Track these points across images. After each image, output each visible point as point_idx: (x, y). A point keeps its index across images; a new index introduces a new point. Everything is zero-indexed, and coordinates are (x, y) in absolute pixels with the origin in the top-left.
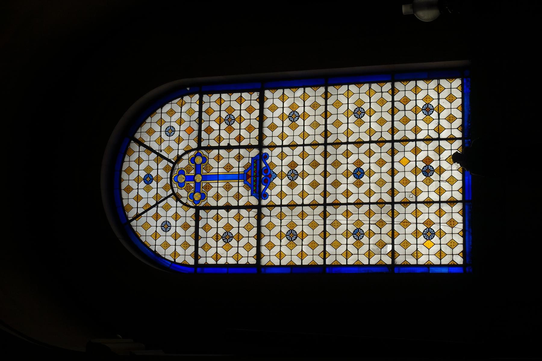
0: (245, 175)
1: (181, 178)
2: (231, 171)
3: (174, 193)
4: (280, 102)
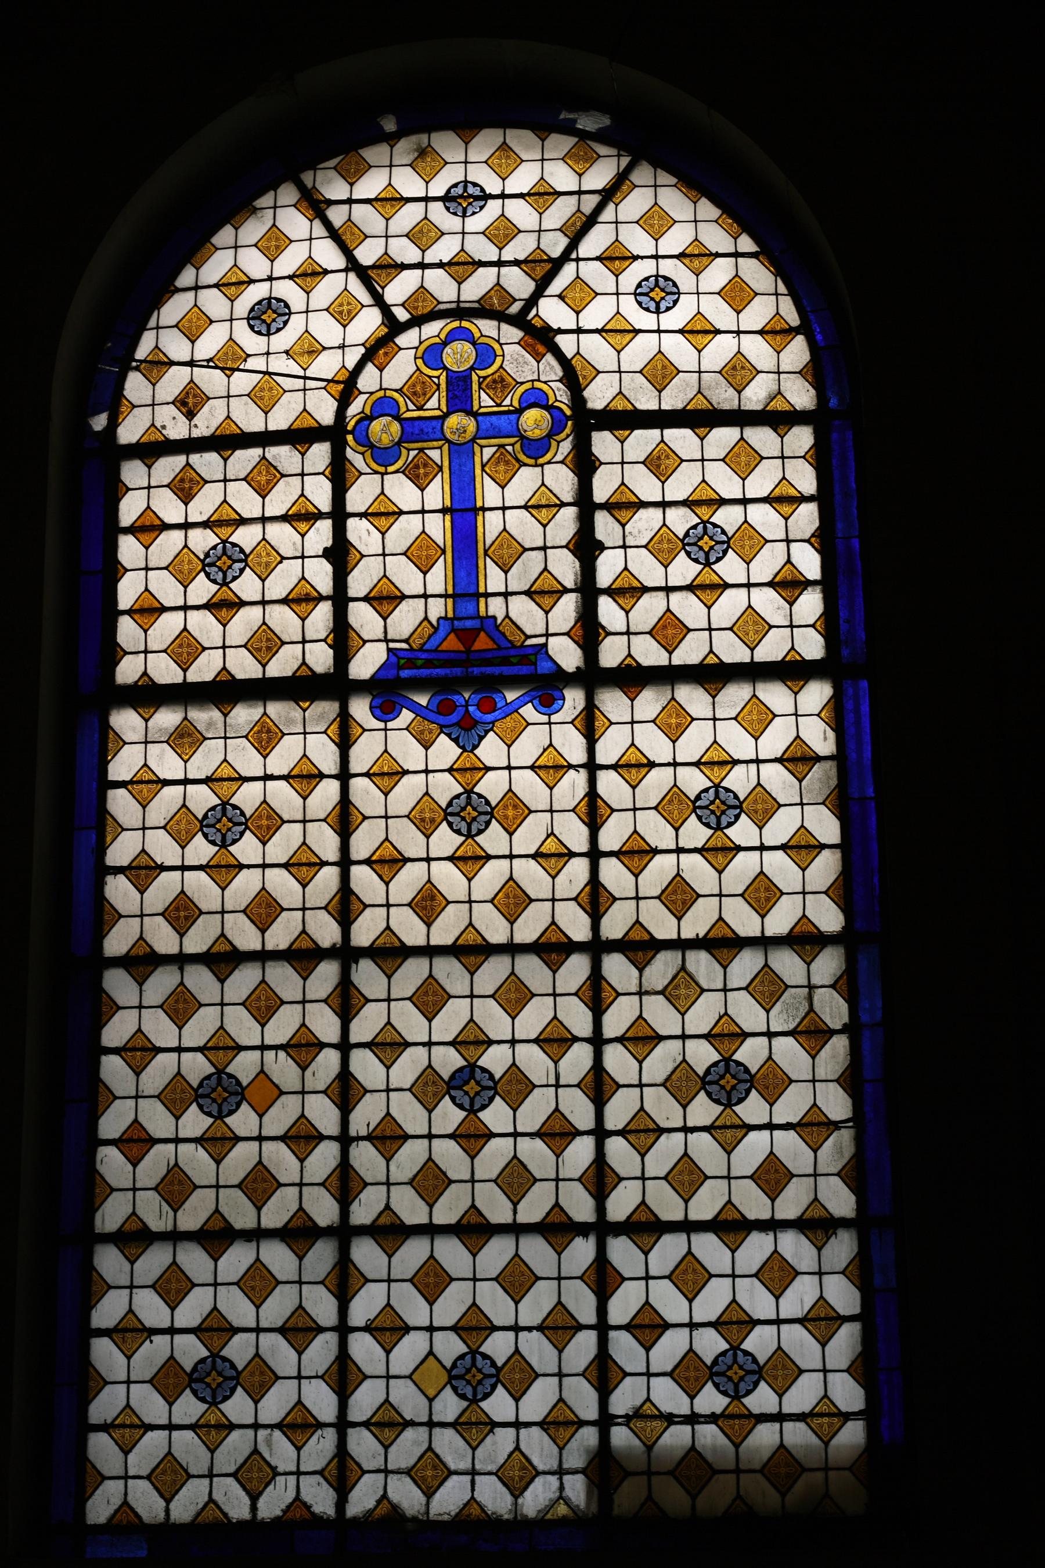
1: (459, 356)
3: (394, 327)
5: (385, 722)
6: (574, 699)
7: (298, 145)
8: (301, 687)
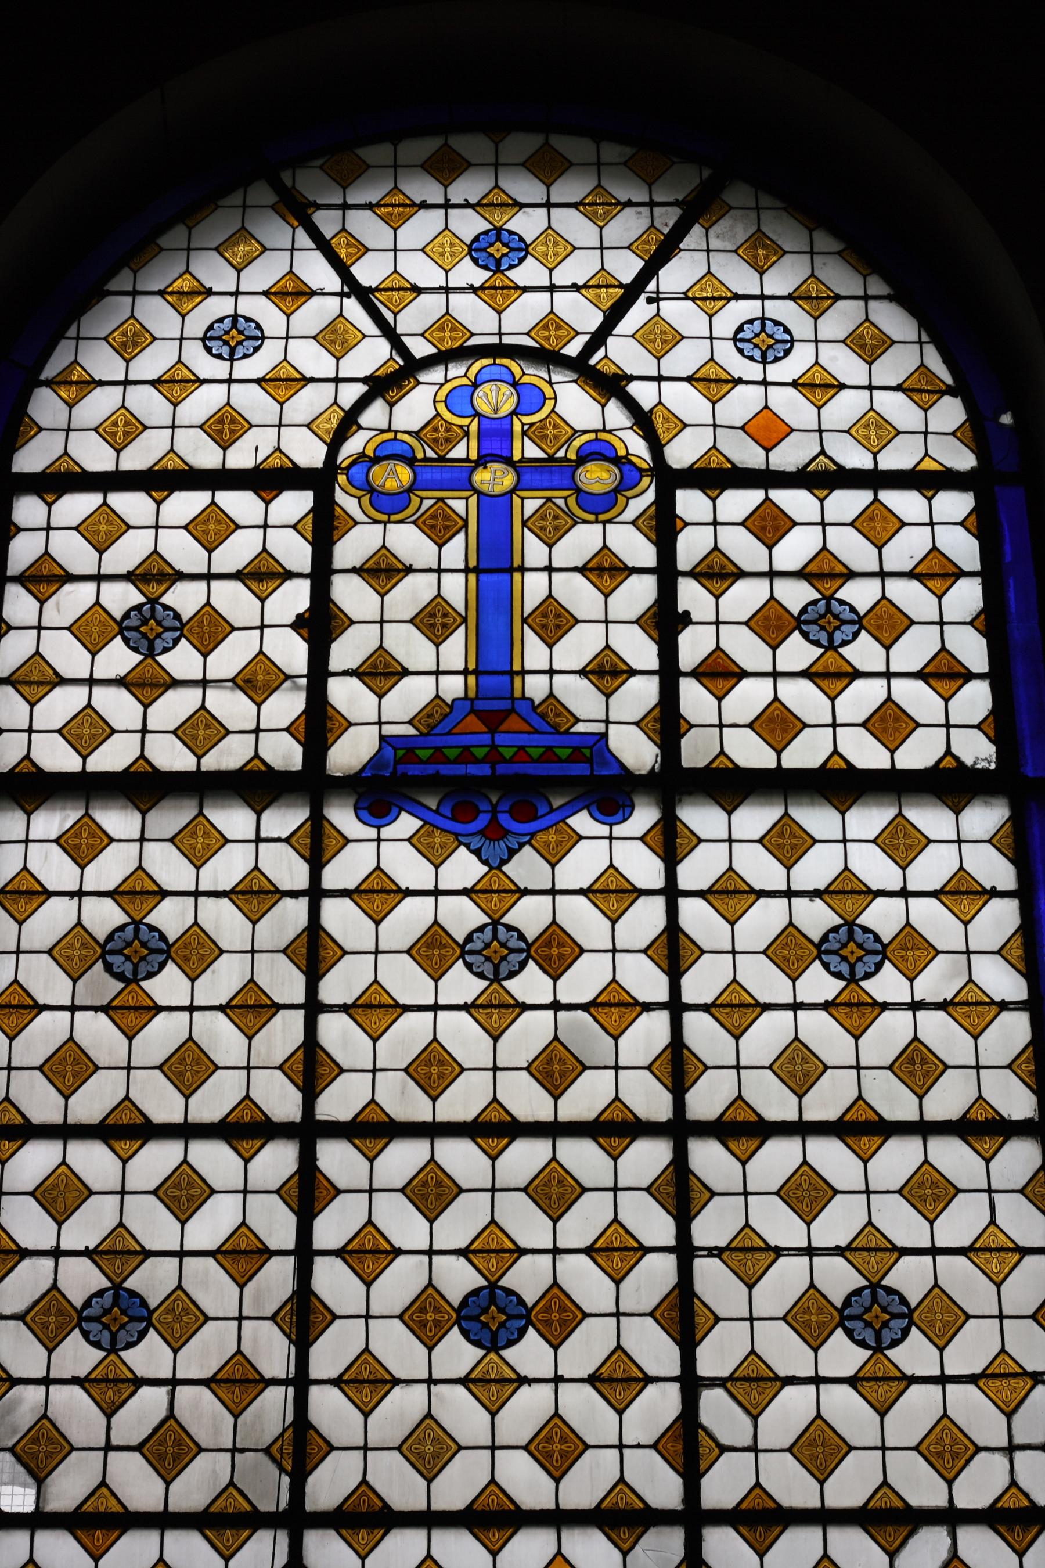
0: (505, 705)
1: (496, 399)
2: (529, 633)
5: (611, 825)
7: (282, 143)
8: (257, 786)
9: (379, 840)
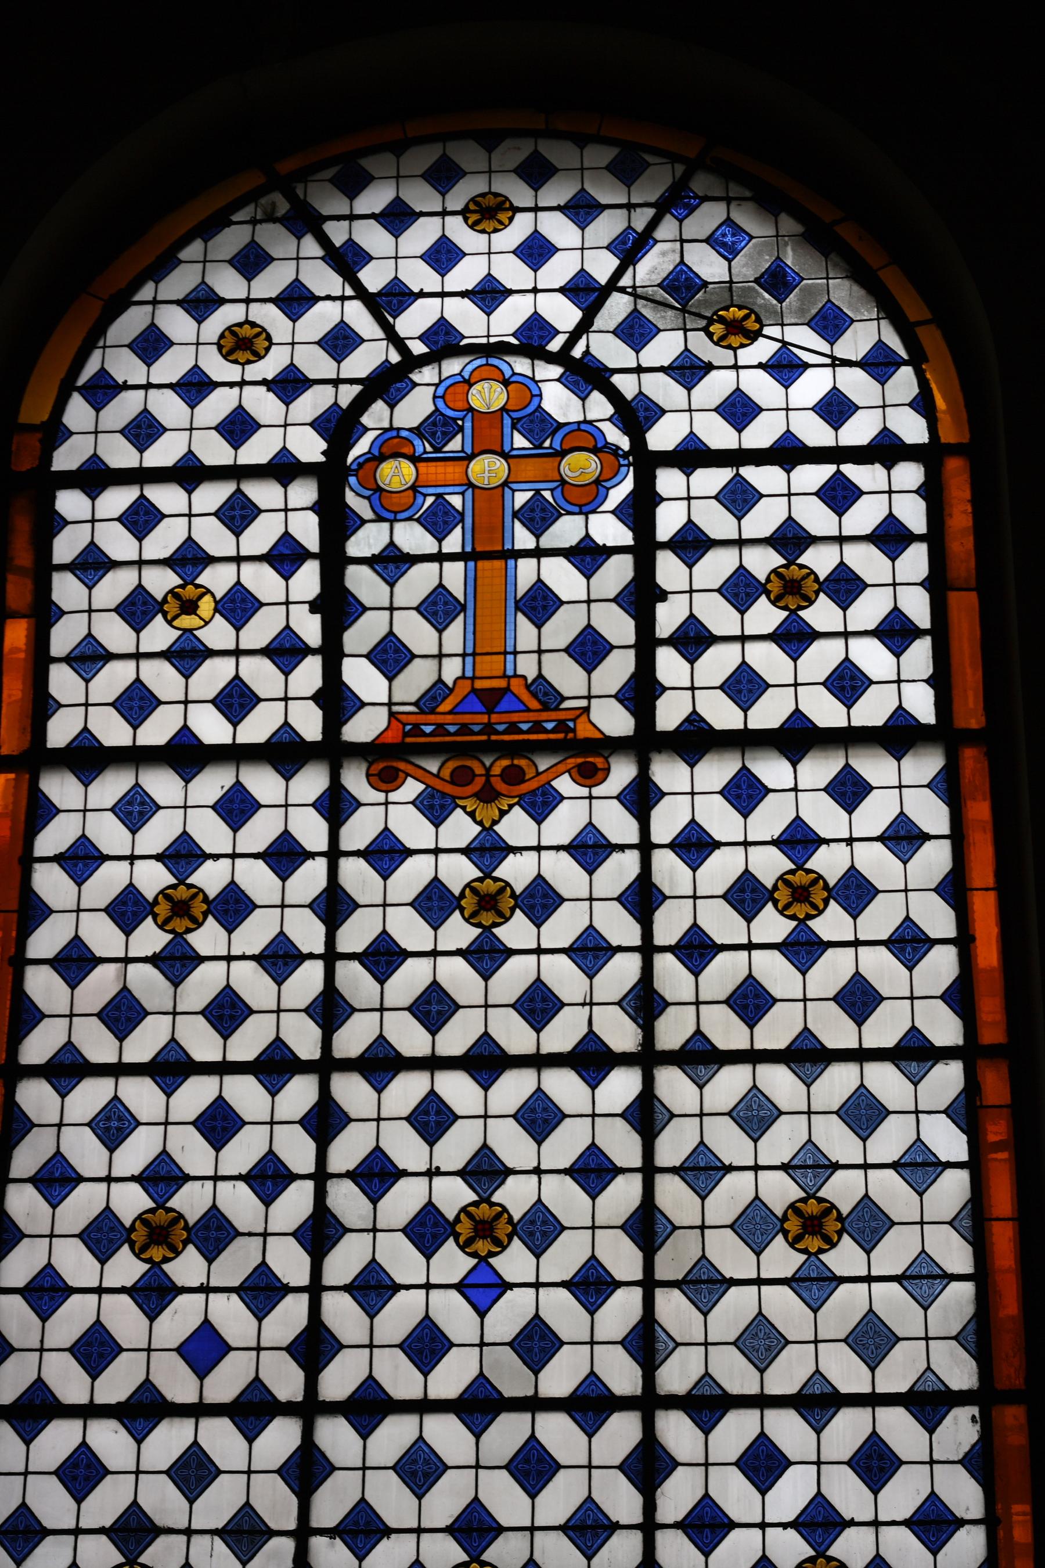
3: (411, 362)
4: (894, 834)
5: (387, 792)
6: (622, 773)
7: (284, 149)
9: (387, 803)
